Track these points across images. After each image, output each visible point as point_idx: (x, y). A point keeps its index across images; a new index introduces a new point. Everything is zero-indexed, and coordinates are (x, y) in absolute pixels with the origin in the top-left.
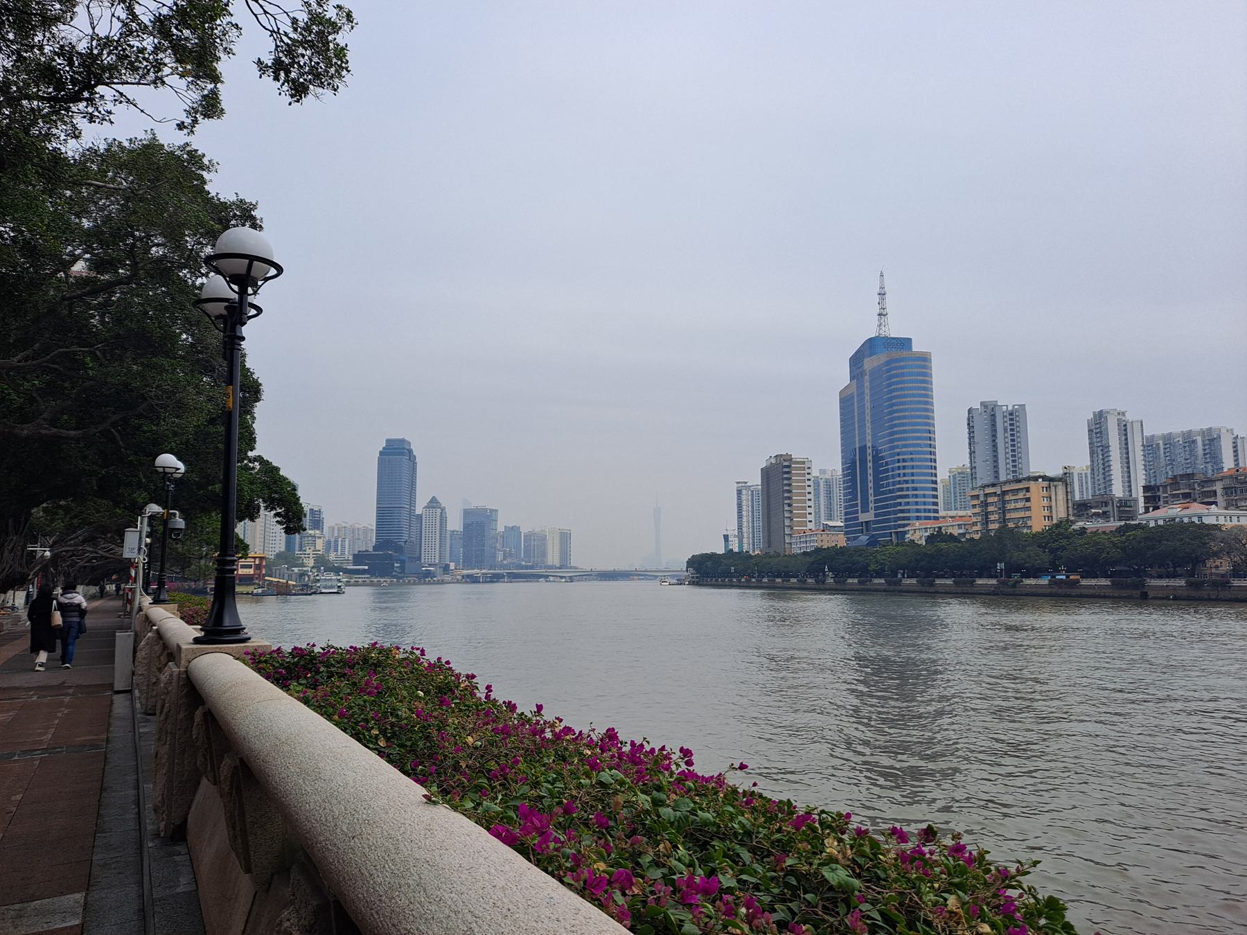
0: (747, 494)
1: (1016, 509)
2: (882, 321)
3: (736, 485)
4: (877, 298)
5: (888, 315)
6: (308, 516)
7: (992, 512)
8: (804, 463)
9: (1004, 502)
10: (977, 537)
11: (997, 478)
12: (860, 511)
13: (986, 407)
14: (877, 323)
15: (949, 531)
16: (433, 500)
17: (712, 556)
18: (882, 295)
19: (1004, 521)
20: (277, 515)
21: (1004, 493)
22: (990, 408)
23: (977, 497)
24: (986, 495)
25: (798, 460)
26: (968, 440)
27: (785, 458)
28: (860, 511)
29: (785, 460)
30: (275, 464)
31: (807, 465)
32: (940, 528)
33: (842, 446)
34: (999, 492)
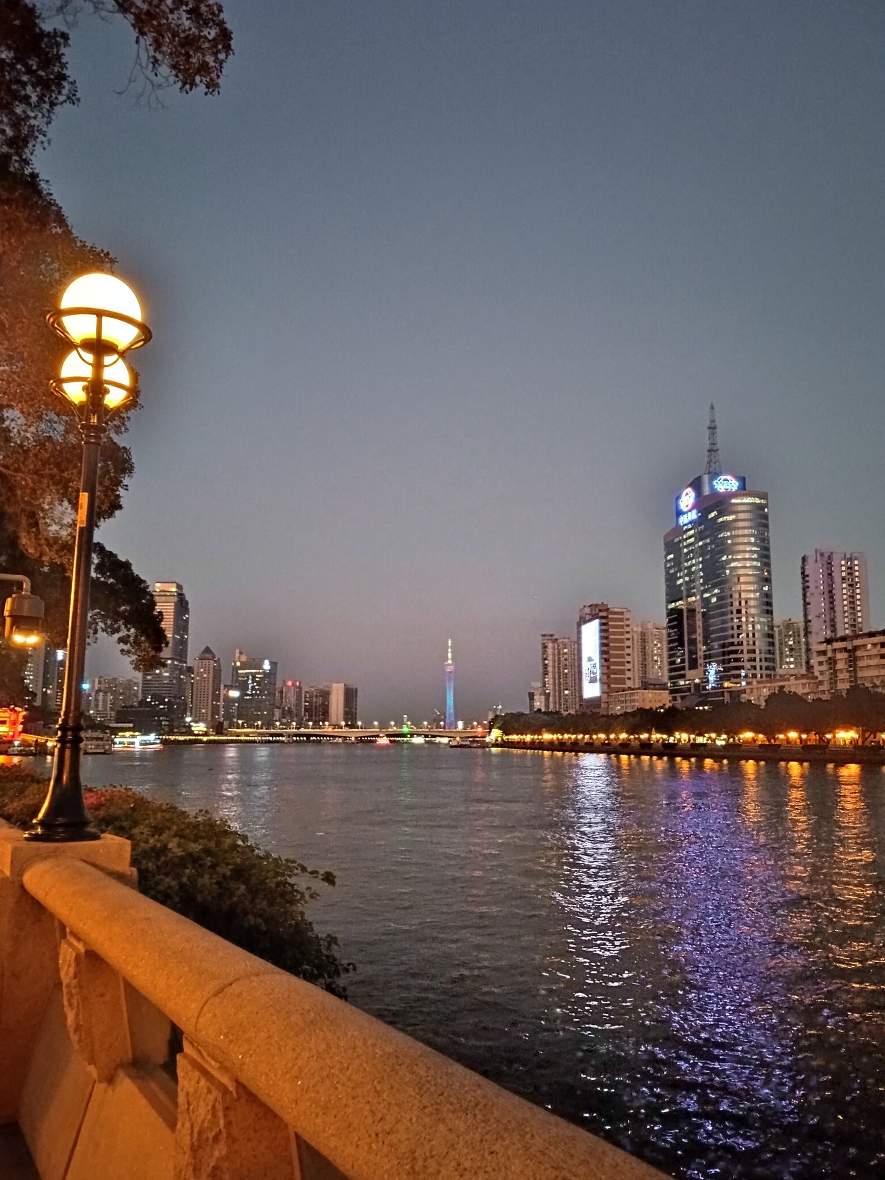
0: (554, 648)
1: (868, 667)
2: (713, 457)
3: (541, 638)
4: (707, 432)
5: (719, 452)
6: (170, 645)
7: (841, 670)
8: (622, 613)
9: (856, 659)
10: (825, 697)
11: (834, 630)
12: (687, 667)
13: (822, 555)
14: (706, 459)
15: (793, 690)
16: (207, 650)
17: (521, 715)
18: (712, 428)
19: (854, 678)
20: (121, 640)
21: (855, 648)
22: (826, 555)
23: (824, 653)
24: (834, 651)
25: (616, 610)
26: (801, 591)
27: (601, 608)
28: (687, 667)
29: (600, 611)
30: (122, 558)
31: (626, 615)
32: (783, 687)
33: (667, 595)
34: (850, 648)
